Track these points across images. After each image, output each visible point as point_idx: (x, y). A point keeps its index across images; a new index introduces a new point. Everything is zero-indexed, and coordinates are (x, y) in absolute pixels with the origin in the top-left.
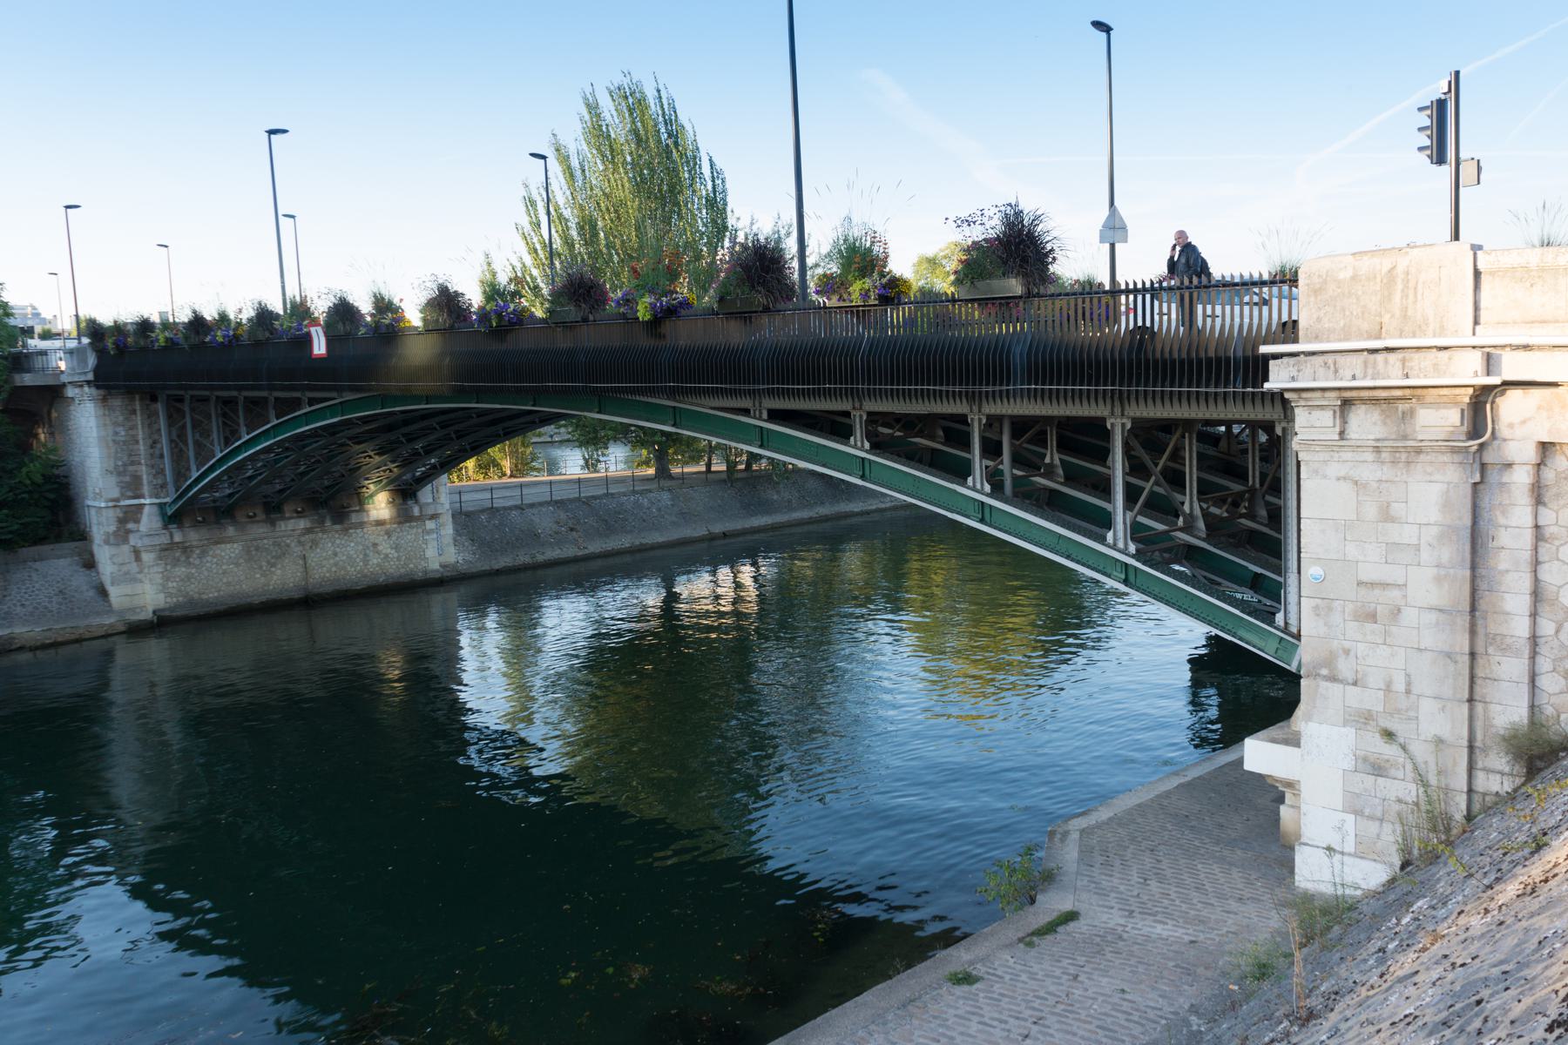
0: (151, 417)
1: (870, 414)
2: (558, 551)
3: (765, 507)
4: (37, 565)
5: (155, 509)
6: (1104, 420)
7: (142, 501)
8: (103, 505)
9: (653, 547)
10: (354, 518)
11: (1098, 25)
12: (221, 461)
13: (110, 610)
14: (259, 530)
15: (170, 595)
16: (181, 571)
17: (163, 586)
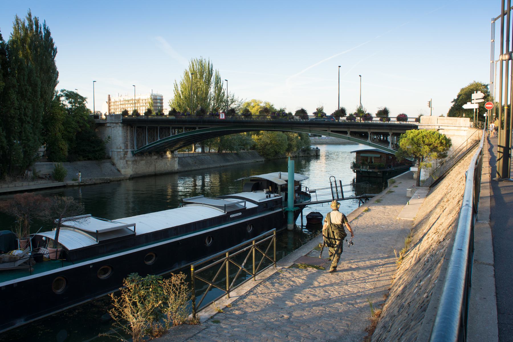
0: (132, 131)
1: (351, 131)
2: (195, 168)
3: (228, 161)
4: (104, 164)
5: (131, 152)
6: (388, 133)
7: (128, 150)
8: (122, 150)
9: (201, 169)
10: (164, 156)
11: (360, 76)
12: (159, 141)
13: (122, 175)
14: (149, 158)
15: (133, 172)
16: (135, 166)
17: (132, 169)
